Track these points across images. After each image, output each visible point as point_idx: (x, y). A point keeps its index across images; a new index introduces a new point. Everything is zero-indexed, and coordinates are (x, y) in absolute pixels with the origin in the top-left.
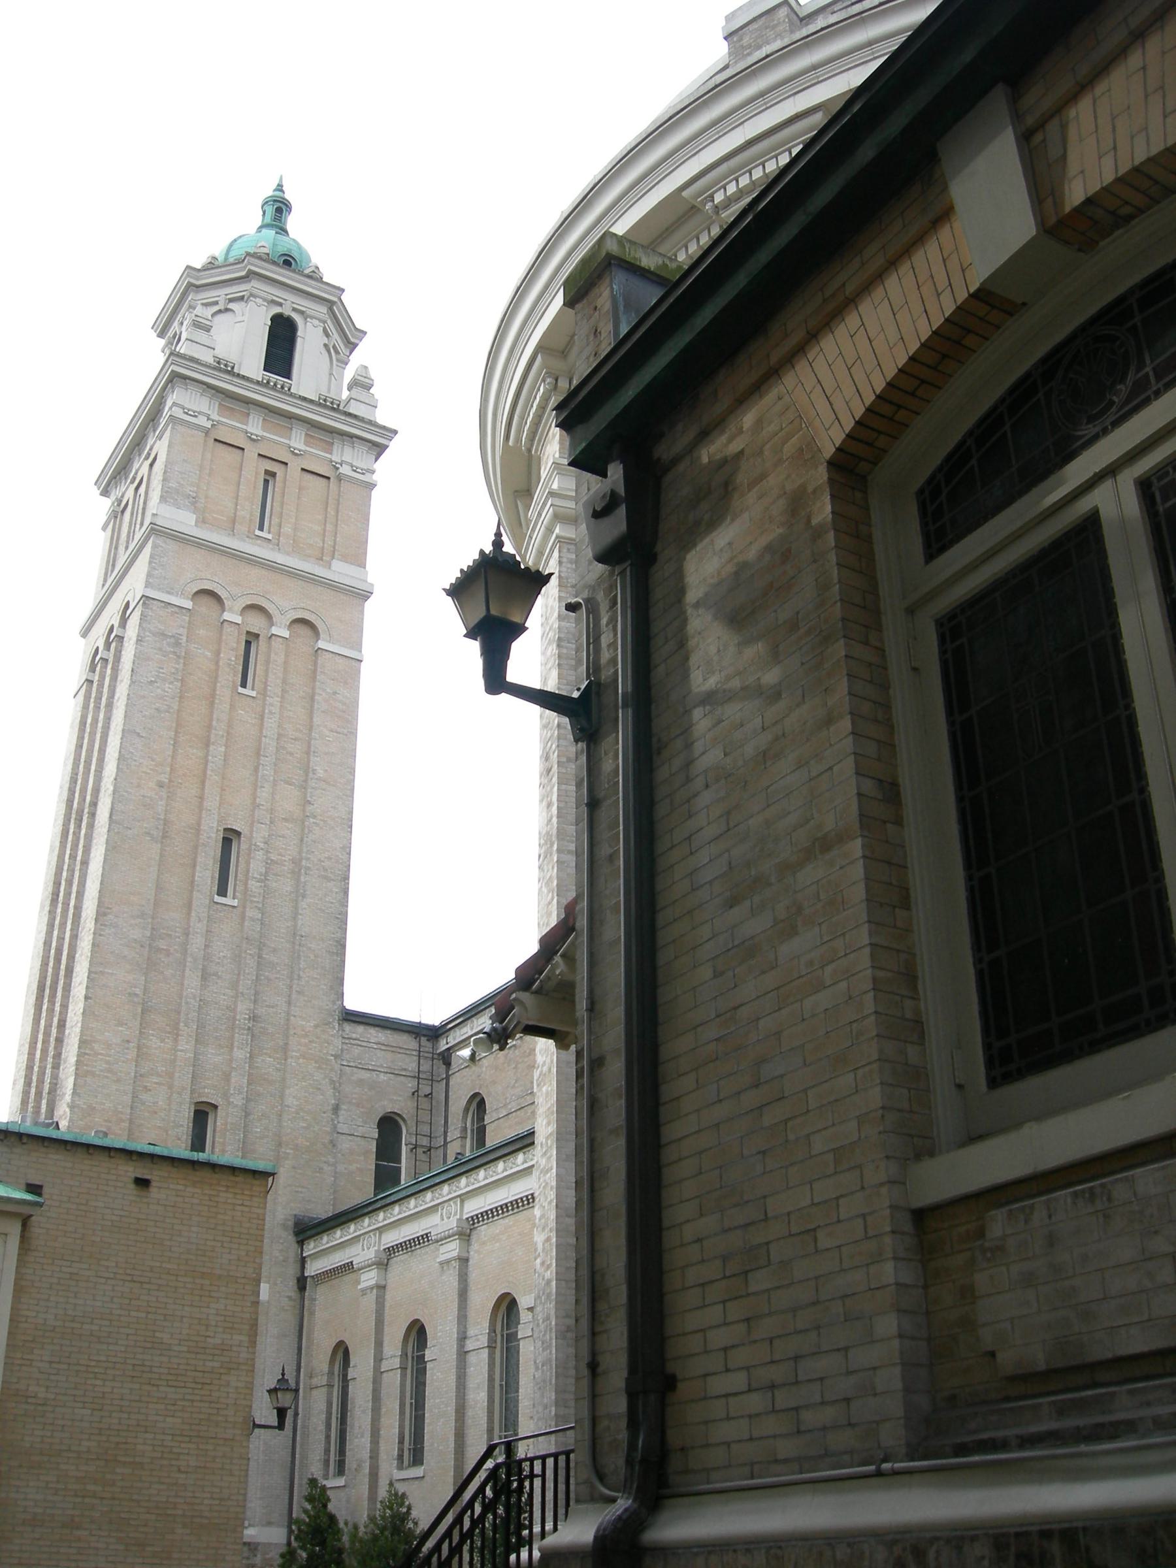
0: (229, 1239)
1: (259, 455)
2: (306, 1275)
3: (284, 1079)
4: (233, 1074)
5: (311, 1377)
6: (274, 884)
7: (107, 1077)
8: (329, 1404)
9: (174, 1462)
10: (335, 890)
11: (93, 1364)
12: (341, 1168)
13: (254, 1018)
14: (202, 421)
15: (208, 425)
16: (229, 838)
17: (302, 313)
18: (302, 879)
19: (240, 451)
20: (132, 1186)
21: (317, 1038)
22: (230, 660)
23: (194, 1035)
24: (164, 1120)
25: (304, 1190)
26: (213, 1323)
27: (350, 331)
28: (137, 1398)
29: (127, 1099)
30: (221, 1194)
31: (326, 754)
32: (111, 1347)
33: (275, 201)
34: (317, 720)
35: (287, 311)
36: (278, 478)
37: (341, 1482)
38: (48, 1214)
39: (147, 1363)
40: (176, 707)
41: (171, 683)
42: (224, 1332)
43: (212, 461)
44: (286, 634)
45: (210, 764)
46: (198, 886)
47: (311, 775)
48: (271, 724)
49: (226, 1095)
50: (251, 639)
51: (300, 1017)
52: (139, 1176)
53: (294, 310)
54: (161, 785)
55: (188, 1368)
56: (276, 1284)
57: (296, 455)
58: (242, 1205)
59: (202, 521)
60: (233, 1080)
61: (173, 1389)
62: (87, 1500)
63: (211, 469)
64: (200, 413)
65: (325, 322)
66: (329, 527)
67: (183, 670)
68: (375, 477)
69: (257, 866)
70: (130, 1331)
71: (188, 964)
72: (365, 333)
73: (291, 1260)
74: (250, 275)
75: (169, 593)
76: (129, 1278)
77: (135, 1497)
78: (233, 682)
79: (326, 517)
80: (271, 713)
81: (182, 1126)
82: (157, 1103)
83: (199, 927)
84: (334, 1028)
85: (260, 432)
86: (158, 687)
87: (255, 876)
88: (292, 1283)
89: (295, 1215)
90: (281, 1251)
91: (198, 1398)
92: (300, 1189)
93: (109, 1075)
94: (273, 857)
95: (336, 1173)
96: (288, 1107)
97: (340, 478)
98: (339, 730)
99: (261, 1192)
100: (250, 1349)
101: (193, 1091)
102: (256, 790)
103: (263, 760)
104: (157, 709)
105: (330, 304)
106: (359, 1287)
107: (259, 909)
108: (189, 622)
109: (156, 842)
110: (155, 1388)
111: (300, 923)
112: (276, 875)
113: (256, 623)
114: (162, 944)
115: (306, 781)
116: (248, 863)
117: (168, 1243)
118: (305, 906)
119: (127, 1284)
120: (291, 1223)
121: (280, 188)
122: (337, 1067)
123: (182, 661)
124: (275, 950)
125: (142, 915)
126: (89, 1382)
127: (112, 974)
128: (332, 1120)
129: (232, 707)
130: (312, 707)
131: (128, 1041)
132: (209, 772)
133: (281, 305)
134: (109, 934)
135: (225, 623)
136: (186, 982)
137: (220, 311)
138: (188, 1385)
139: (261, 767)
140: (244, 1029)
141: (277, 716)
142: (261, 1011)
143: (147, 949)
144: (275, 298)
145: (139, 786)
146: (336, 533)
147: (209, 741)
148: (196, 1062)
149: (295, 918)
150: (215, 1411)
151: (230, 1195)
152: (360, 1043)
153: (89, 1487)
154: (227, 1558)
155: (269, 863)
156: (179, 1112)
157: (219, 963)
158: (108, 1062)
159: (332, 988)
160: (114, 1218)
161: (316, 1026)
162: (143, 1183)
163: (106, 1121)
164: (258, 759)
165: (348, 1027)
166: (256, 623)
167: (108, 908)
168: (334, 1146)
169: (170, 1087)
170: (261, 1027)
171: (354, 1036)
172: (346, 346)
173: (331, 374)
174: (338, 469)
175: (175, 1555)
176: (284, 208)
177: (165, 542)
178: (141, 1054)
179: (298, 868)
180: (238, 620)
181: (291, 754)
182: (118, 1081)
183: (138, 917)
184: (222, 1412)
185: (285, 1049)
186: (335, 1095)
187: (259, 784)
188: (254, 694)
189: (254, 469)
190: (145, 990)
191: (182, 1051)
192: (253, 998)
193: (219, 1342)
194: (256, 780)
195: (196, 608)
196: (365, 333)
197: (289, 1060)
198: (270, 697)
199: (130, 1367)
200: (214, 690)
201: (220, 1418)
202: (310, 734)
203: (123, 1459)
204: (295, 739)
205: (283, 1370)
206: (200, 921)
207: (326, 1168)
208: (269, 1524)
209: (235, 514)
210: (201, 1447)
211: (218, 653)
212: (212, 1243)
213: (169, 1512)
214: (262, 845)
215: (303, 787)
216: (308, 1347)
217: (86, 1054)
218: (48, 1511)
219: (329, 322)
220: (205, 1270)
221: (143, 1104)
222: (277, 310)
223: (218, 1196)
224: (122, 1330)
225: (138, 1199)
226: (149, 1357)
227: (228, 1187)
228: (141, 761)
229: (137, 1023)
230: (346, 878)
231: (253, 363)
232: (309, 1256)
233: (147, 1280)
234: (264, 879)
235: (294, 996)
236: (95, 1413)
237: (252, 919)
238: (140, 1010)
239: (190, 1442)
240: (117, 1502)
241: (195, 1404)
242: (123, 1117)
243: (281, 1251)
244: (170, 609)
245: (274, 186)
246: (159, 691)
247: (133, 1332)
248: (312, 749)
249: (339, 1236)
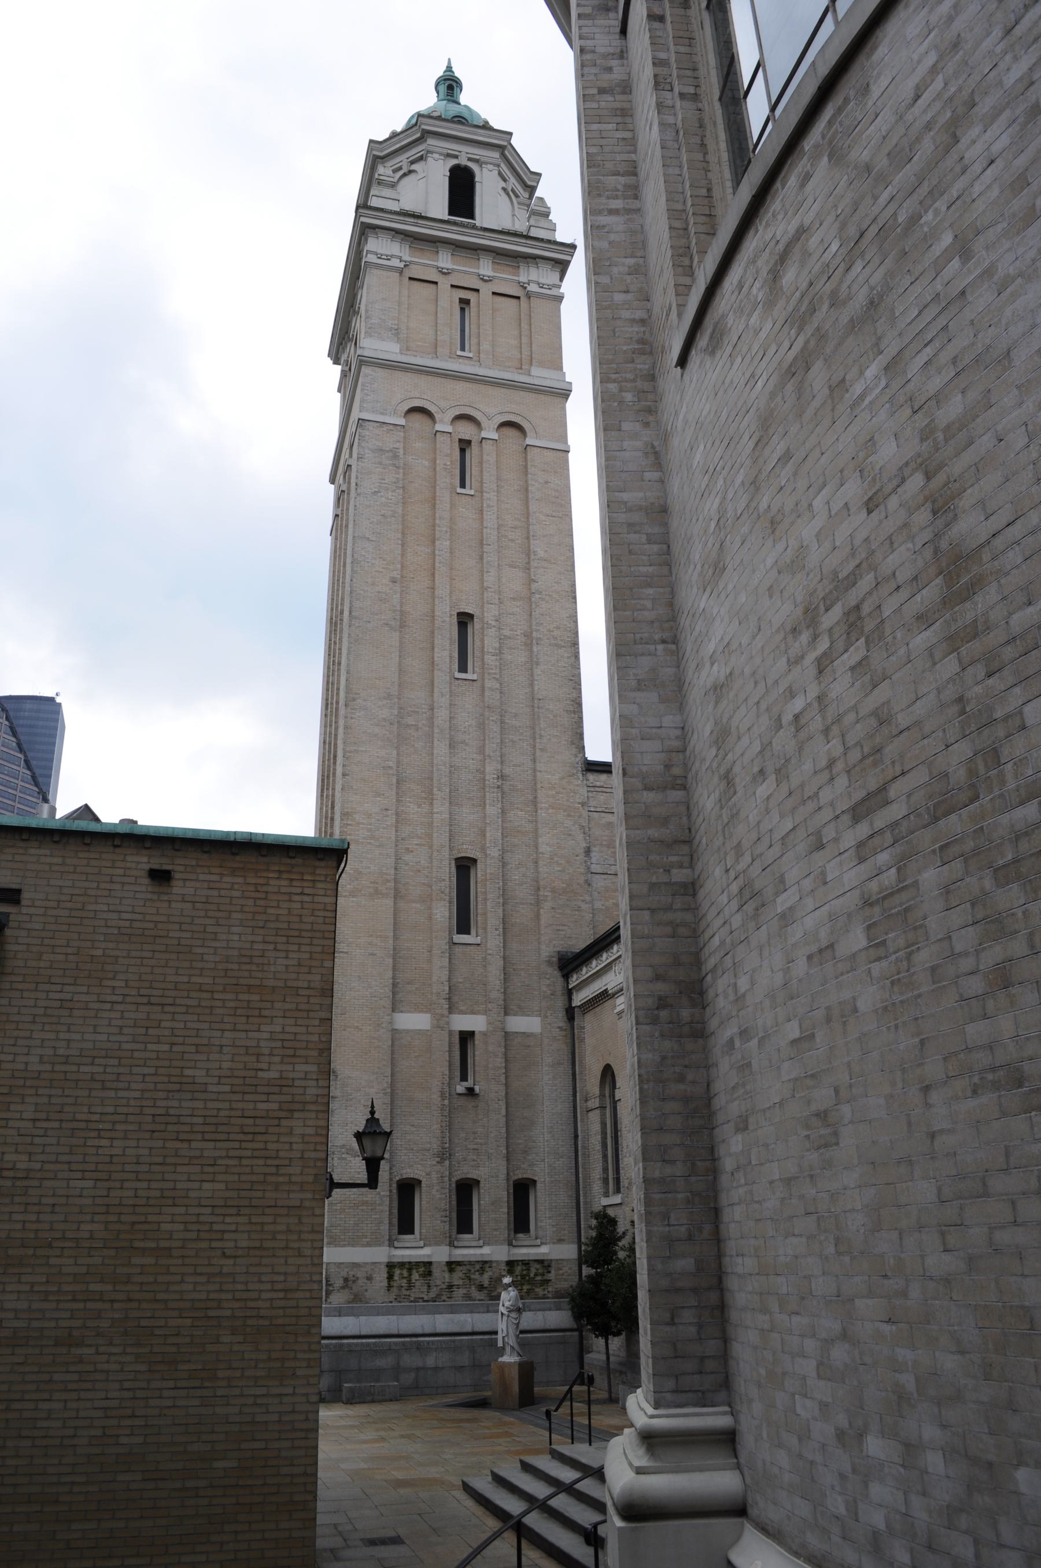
0: (284, 939)
1: (452, 286)
2: (573, 1005)
3: (536, 830)
4: (488, 829)
5: (586, 1101)
6: (510, 657)
7: (370, 843)
8: (603, 1124)
9: (214, 1244)
10: (566, 655)
11: (96, 1117)
12: (598, 905)
13: (502, 777)
14: (395, 263)
15: (402, 265)
16: (464, 620)
17: (477, 161)
18: (535, 649)
19: (433, 286)
20: (146, 881)
21: (564, 789)
22: (445, 465)
23: (447, 797)
24: (427, 876)
25: (564, 928)
26: (267, 1051)
27: (526, 174)
28: (160, 1160)
29: (391, 861)
30: (272, 882)
31: (544, 536)
32: (121, 1094)
33: (445, 80)
34: (533, 507)
35: (463, 161)
36: (472, 304)
37: (617, 1199)
38: (29, 926)
39: (172, 1112)
40: (400, 512)
41: (394, 491)
42: (282, 1062)
43: (409, 297)
44: (495, 436)
45: (437, 558)
46: (438, 665)
47: (532, 557)
48: (490, 518)
49: (483, 849)
50: (464, 445)
51: (546, 772)
52: (156, 867)
53: (470, 159)
54: (394, 581)
55: (233, 1113)
56: (547, 1017)
57: (486, 281)
58: (302, 894)
59: (406, 349)
60: (488, 835)
61: (211, 1145)
62: (90, 1305)
63: (409, 304)
64: (392, 256)
65: (499, 166)
66: (525, 340)
67: (404, 479)
68: (561, 290)
69: (491, 642)
70: (146, 1071)
71: (435, 735)
72: (539, 175)
73: (559, 993)
74: (426, 134)
75: (382, 414)
76: (145, 1000)
77: (161, 1296)
79: (520, 332)
80: (489, 506)
81: (444, 880)
82: (420, 862)
83: (442, 701)
84: (579, 779)
85: (450, 266)
86: (382, 496)
87: (490, 650)
88: (561, 1014)
89: (559, 952)
90: (548, 986)
91: (249, 1153)
92: (561, 928)
93: (372, 841)
94: (506, 632)
95: (593, 910)
96: (542, 853)
97: (529, 296)
98: (554, 514)
99: (326, 876)
100: (321, 1083)
101: (451, 849)
102: (482, 575)
103: (486, 548)
104: (382, 515)
105: (501, 148)
106: (616, 1011)
107: (497, 679)
108: (405, 438)
109: (395, 631)
110: (185, 1145)
111: (536, 688)
112: (511, 648)
113: (466, 431)
114: (410, 721)
115: (528, 563)
116: (482, 641)
117: (200, 950)
118: (539, 673)
119: (142, 1008)
120: (555, 959)
121: (449, 68)
122: (585, 814)
123: (401, 471)
124: (516, 715)
125: (389, 697)
126: (89, 1143)
127: (366, 751)
128: (585, 862)
129: (453, 506)
130: (527, 497)
131: (387, 810)
132: (437, 565)
134: (359, 717)
135: (438, 433)
136: (435, 752)
138: (232, 1137)
139: (485, 554)
140: (494, 788)
141: (495, 509)
142: (507, 771)
143: (396, 726)
144: (449, 152)
145: (373, 584)
147: (434, 538)
148: (451, 822)
149: (532, 685)
150: (273, 1170)
151: (284, 883)
152: (604, 790)
153: (93, 1287)
154: (299, 1372)
155: (502, 639)
156: (440, 868)
157: (465, 732)
158: (370, 830)
159: (572, 743)
160: (122, 923)
161: (562, 778)
162: (160, 877)
163: (372, 883)
164: (482, 547)
165: (591, 777)
166: (466, 431)
167: (356, 694)
168: (589, 885)
169: (431, 847)
170: (510, 785)
171: (598, 784)
172: (524, 190)
173: (514, 215)
174: (525, 288)
175: (220, 1374)
176: (454, 84)
177: (375, 371)
178: (400, 819)
179: (529, 640)
180: (449, 429)
181: (512, 541)
182: (381, 845)
183: (385, 698)
184: (282, 1171)
185: (535, 802)
186: (585, 839)
187: (485, 570)
188: (472, 492)
189: (449, 299)
190: (398, 762)
191: (437, 813)
192: (499, 759)
193: (276, 1075)
194: (482, 567)
196: (539, 175)
197: (539, 811)
198: (486, 492)
199: (149, 1119)
201: (281, 1179)
202: (528, 521)
203: (141, 1244)
204: (515, 528)
205: (373, 1107)
206: (442, 695)
207: (584, 906)
208: (560, 1241)
209: (436, 340)
210: (254, 1219)
211: (434, 461)
212: (261, 946)
213: (211, 1313)
214: (493, 623)
215: (527, 568)
216: (581, 1073)
217: (348, 825)
218: (35, 1324)
219: (502, 165)
220: (252, 982)
221: (407, 864)
222: (454, 162)
223: (267, 884)
224: (135, 1070)
225: (155, 897)
226: (175, 1104)
227: (280, 872)
228: (373, 561)
229: (394, 792)
230: (575, 644)
231: (439, 207)
232: (574, 987)
233: (170, 1001)
234: (500, 652)
235: (538, 753)
236: (99, 1184)
237: (491, 689)
238: (394, 781)
239: (238, 1215)
240: (135, 1305)
241: (244, 1162)
242: (388, 877)
243: (548, 986)
244: (385, 428)
245: (444, 68)
246: (383, 499)
247: (152, 1071)
248: (531, 534)
249: (595, 965)
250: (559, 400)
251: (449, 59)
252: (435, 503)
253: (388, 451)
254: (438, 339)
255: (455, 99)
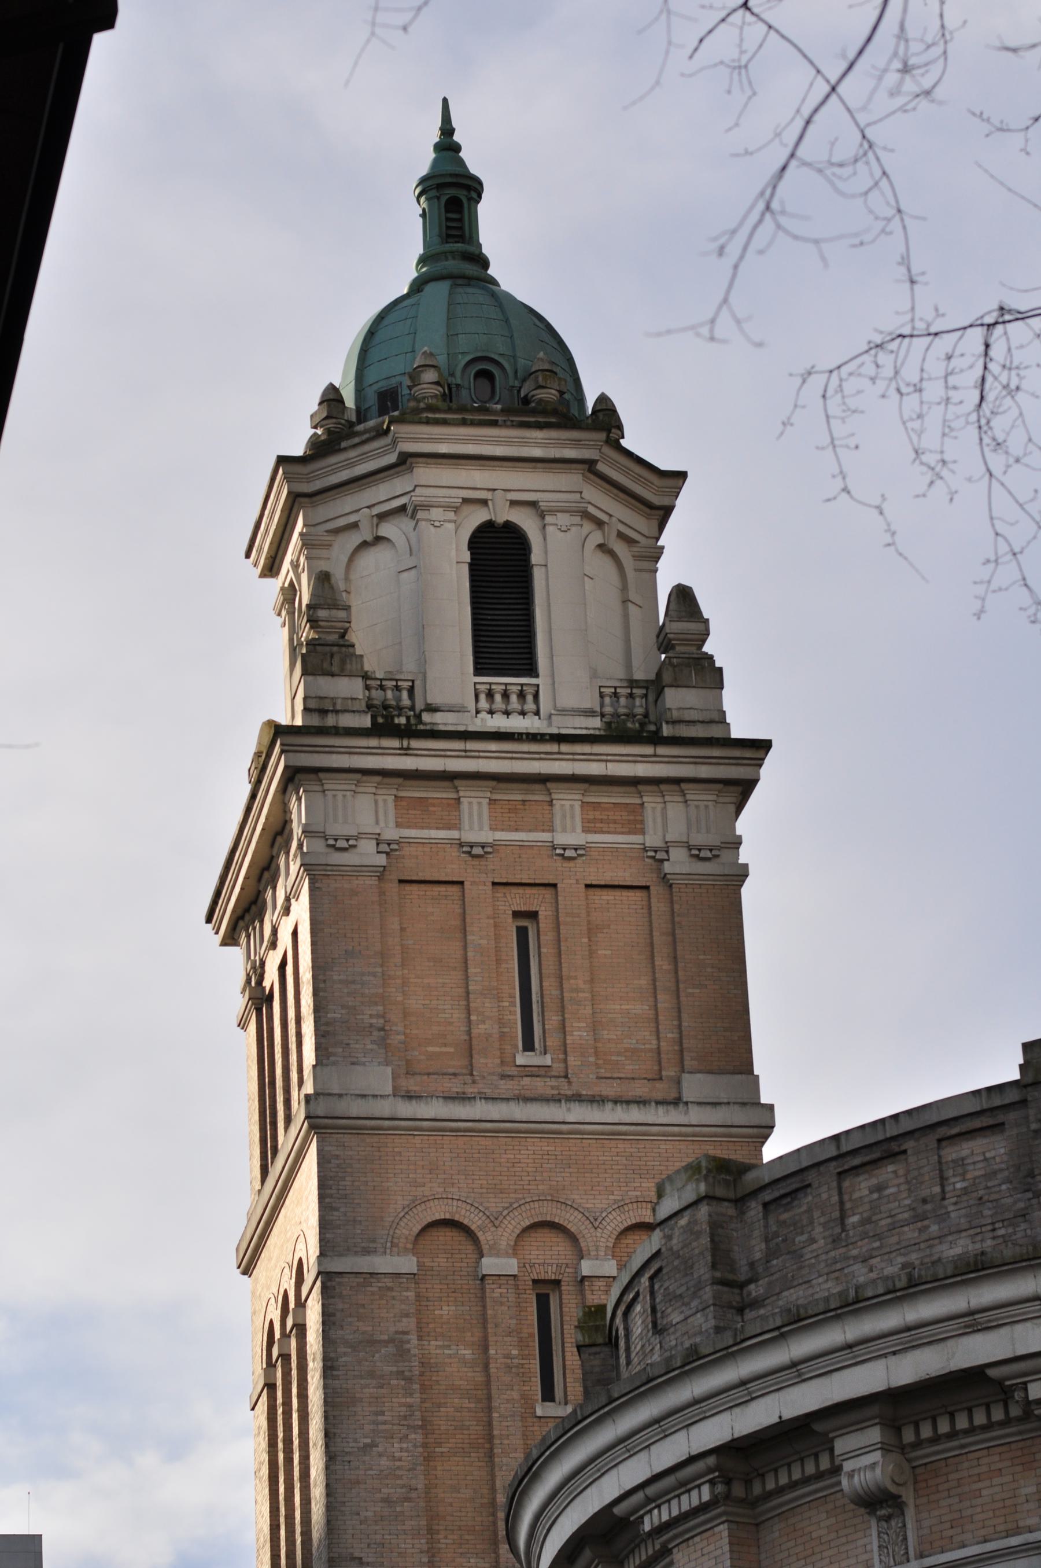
22: (508, 1356)
33: (440, 186)
35: (503, 514)
57: (571, 859)
78: (524, 1396)
79: (654, 980)
85: (486, 836)
133: (484, 502)
135: (488, 1280)
137: (365, 545)
146: (679, 1011)
176: (462, 194)
195: (427, 1262)
200: (490, 1424)
209: (469, 1033)
211: (484, 1346)
246: (384, 1462)
250: (717, 690)
251: (445, 101)
252: (492, 1449)
253: (386, 1343)
254: (475, 1032)
255: (471, 249)
